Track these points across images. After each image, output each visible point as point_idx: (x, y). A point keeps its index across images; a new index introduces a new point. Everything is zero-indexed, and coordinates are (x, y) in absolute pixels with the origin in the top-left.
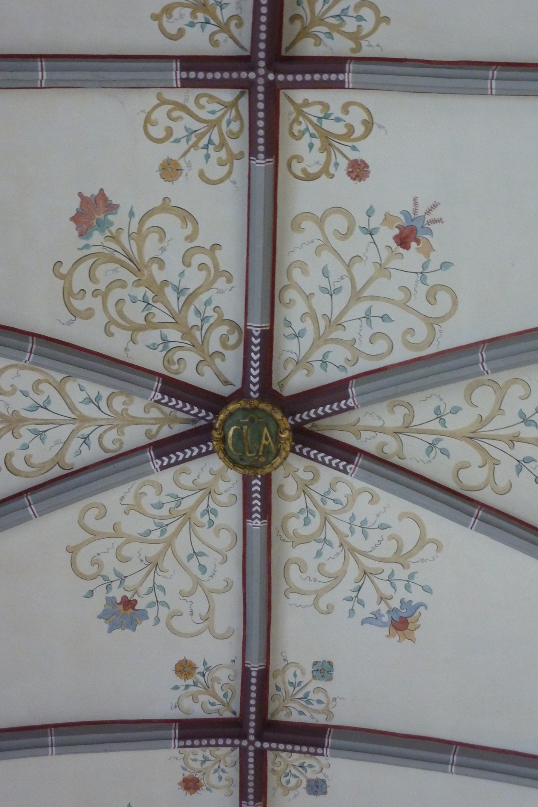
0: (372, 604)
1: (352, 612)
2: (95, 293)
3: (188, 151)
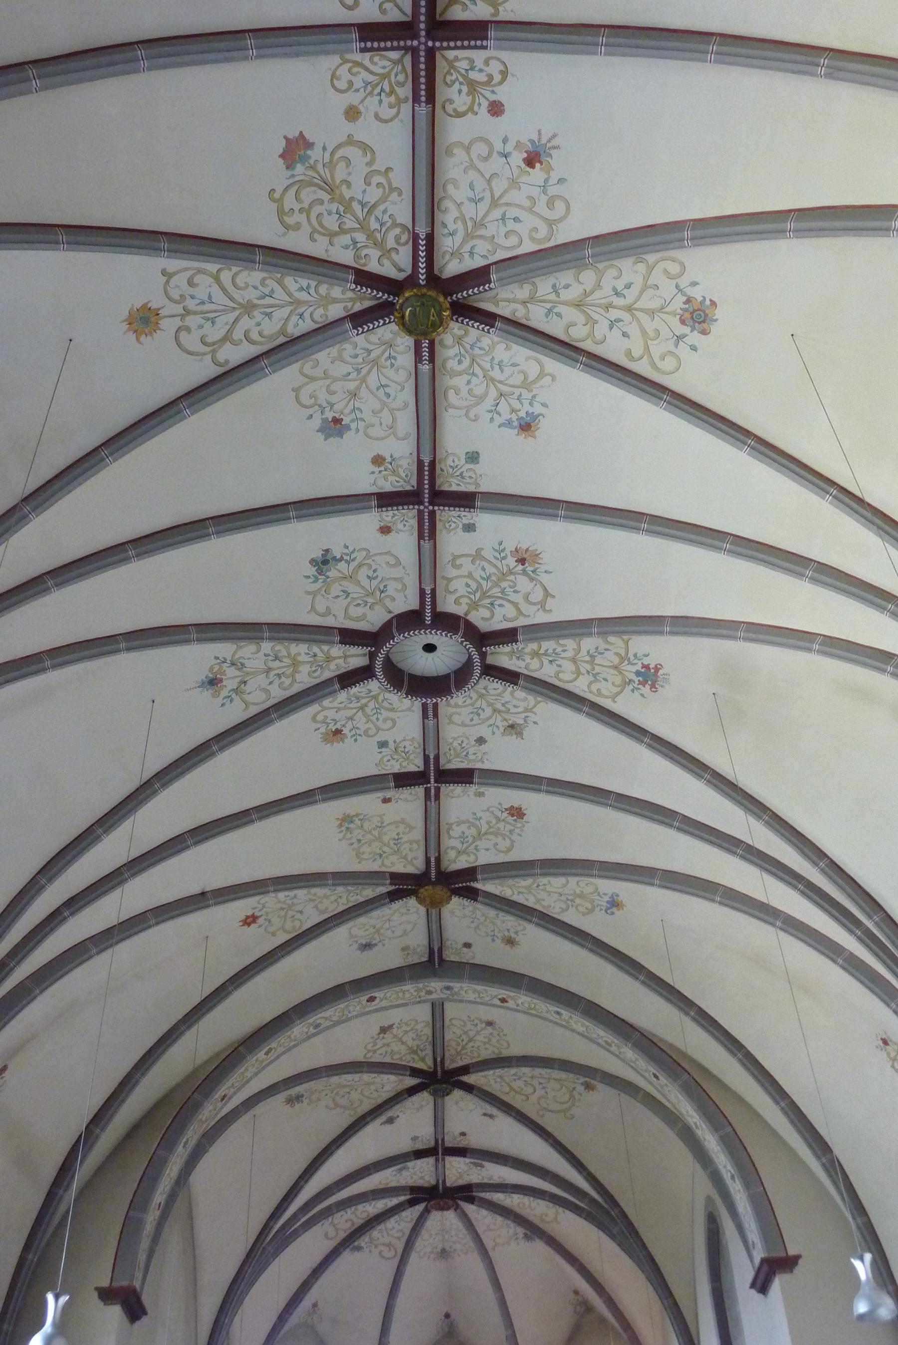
0: (506, 415)
1: (492, 419)
2: (301, 211)
3: (365, 98)
